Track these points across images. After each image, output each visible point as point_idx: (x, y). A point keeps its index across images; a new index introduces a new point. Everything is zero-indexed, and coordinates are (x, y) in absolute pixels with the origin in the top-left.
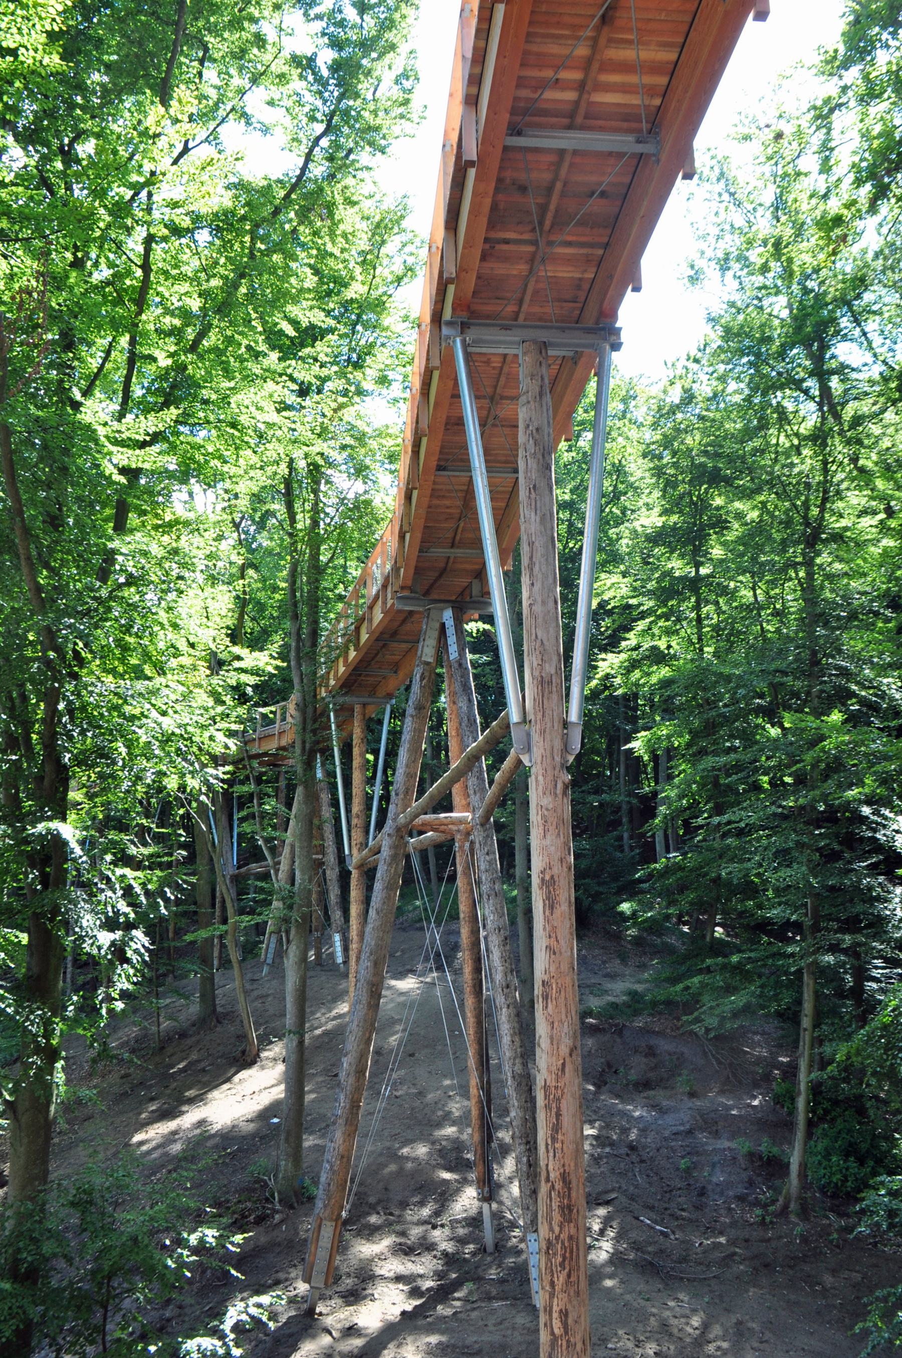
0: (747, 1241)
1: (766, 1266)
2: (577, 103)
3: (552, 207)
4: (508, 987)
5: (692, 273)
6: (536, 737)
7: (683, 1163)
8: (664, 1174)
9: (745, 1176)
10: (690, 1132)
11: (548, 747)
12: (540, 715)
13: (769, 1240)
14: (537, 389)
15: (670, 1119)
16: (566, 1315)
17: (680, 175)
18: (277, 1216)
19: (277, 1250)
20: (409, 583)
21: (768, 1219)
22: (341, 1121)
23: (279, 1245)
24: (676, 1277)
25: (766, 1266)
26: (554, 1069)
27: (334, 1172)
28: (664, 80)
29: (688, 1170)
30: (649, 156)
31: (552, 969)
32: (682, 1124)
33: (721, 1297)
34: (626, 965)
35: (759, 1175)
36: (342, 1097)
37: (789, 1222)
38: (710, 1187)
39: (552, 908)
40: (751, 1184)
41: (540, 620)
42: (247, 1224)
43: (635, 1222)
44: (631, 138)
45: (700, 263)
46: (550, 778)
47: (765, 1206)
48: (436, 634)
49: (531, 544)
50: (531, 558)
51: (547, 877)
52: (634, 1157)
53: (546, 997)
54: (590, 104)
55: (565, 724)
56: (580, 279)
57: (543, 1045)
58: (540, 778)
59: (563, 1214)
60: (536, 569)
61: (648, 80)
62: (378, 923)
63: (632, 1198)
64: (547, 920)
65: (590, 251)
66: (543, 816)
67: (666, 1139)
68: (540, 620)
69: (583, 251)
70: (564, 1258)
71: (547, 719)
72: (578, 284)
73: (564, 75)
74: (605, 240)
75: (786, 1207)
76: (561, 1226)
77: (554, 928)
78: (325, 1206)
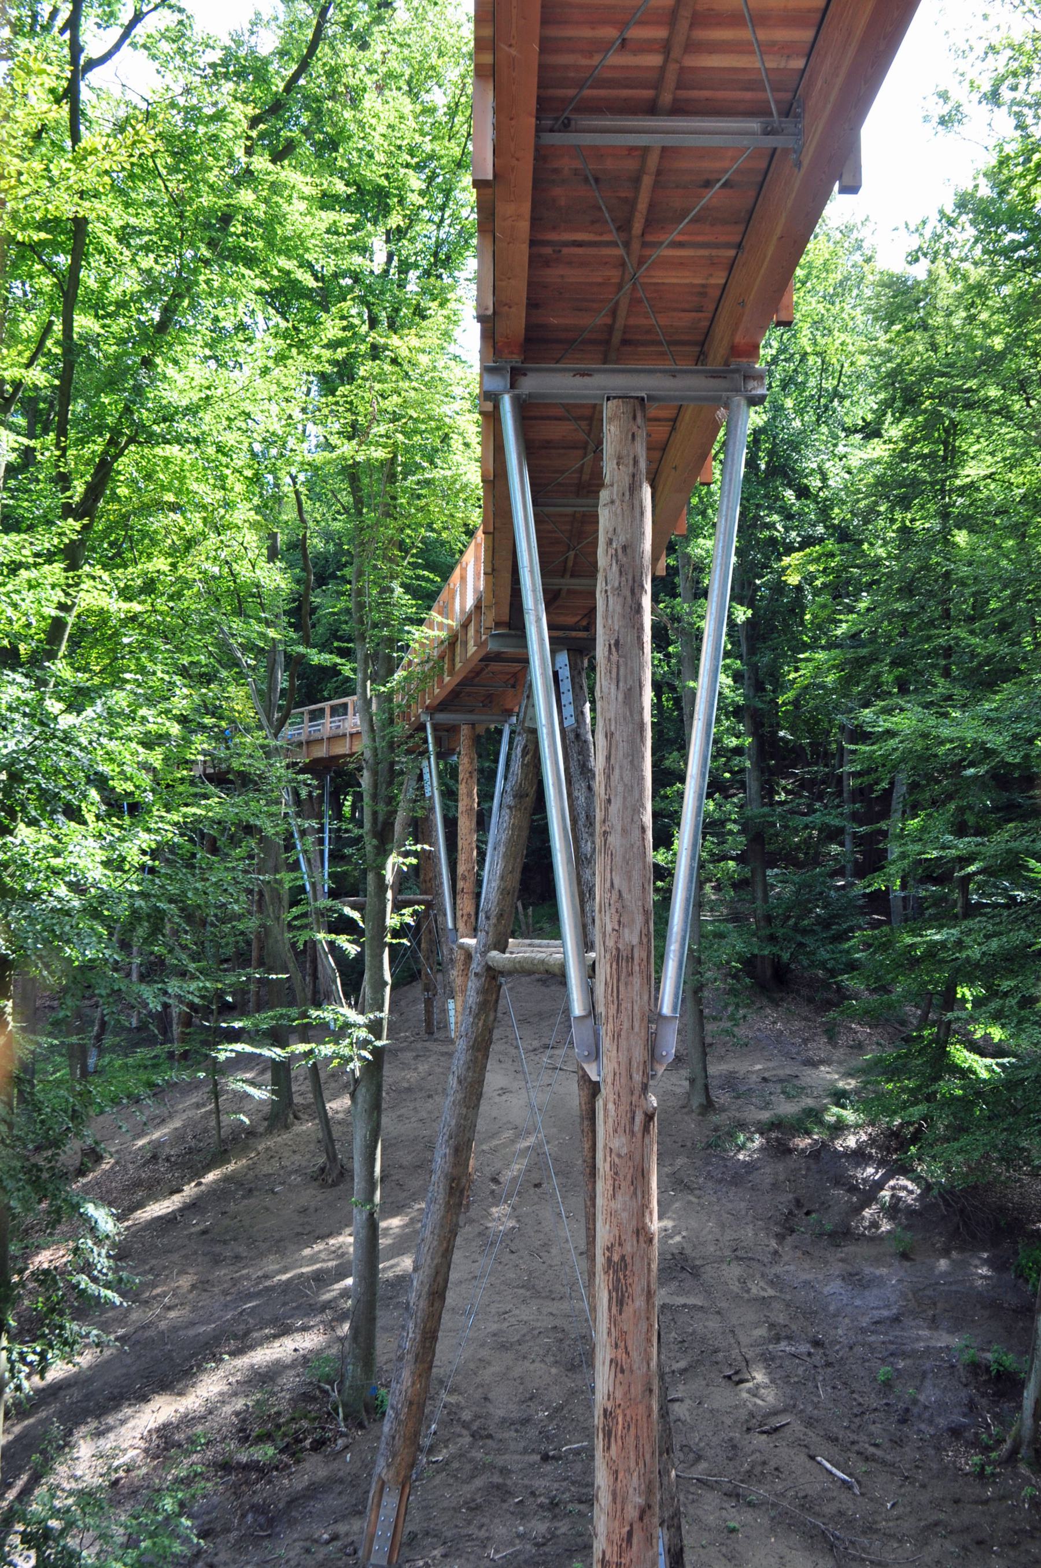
0: (957, 1501)
1: (980, 1543)
2: (663, 69)
3: (642, 206)
5: (945, 110)
6: (606, 1043)
7: (884, 1371)
8: (855, 1385)
9: (963, 1394)
10: (896, 1319)
11: (623, 1059)
12: (613, 1010)
13: (986, 1502)
14: (627, 480)
15: (872, 1297)
17: (836, 187)
18: (340, 1442)
19: (338, 1488)
20: (506, 618)
21: (989, 1469)
22: (409, 1357)
23: (341, 1481)
25: (980, 1543)
26: (616, 1537)
27: (400, 1422)
28: (808, 35)
29: (887, 1384)
30: (786, 151)
31: (619, 1394)
32: (887, 1307)
34: (835, 1046)
35: (984, 1395)
36: (411, 1325)
37: (1017, 1475)
38: (915, 1410)
39: (621, 1303)
40: (971, 1407)
41: (618, 859)
42: (303, 1450)
43: (809, 1464)
44: (754, 125)
45: (959, 94)
46: (624, 1107)
47: (987, 1449)
49: (609, 736)
50: (608, 758)
51: (616, 1258)
53: (608, 1434)
54: (682, 70)
55: (655, 1017)
56: (704, 286)
57: (603, 1501)
58: (611, 1106)
60: (616, 775)
61: (782, 35)
62: (459, 1096)
63: (810, 1423)
64: (613, 1321)
65: (714, 252)
66: (613, 1165)
67: (863, 1331)
68: (618, 859)
69: (705, 252)
71: (624, 1017)
72: (702, 291)
73: (635, 33)
74: (737, 239)
75: (1014, 1451)
77: (623, 1333)
78: (389, 1466)
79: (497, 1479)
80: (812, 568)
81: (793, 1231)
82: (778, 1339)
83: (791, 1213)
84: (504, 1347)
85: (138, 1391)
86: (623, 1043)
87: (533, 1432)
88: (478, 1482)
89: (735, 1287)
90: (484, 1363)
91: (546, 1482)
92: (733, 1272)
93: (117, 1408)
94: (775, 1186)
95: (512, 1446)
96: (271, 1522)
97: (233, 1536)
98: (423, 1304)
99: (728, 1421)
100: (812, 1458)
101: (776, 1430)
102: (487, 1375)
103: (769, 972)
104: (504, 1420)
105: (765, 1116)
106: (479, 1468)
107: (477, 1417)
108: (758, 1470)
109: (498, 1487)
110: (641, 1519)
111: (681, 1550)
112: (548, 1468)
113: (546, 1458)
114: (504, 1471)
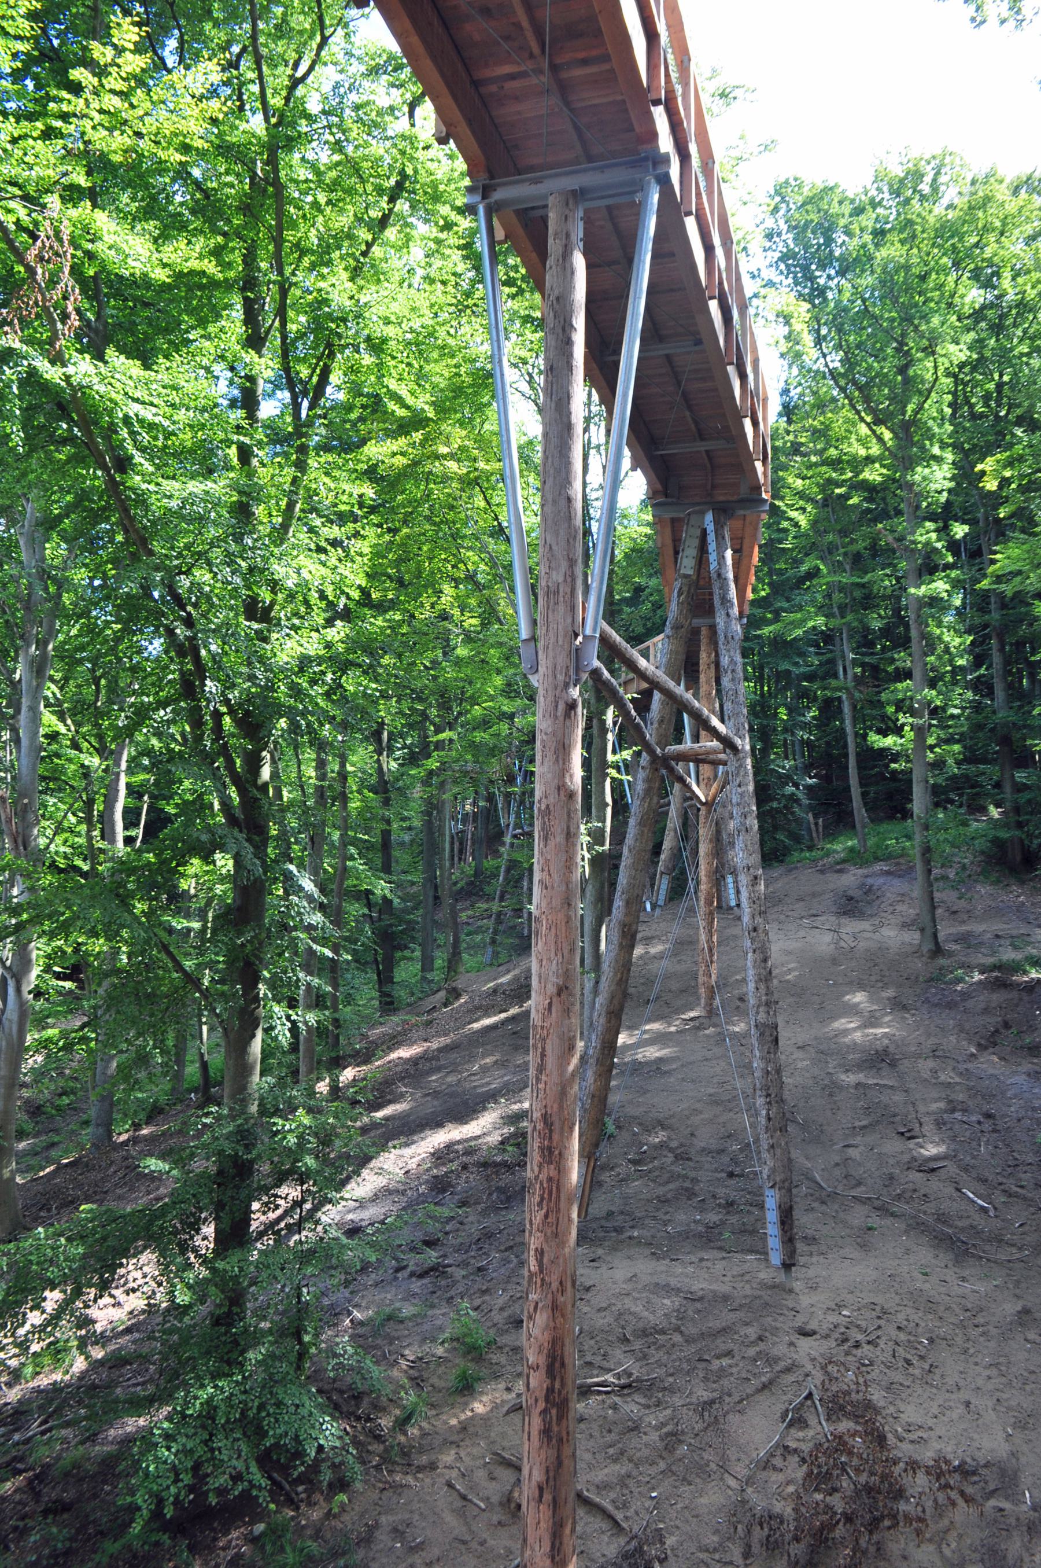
4: (755, 930)
16: (542, 1253)
24: (973, 1255)
33: (1017, 1283)
43: (956, 1194)
46: (550, 698)
48: (696, 542)
52: (987, 1126)
59: (543, 1156)
70: (542, 1199)
76: (540, 1166)
79: (687, 1184)
80: (1007, 474)
81: (995, 1044)
82: (953, 1111)
83: (997, 1031)
84: (716, 1103)
85: (436, 1123)
86: (551, 653)
87: (726, 1159)
88: (671, 1186)
89: (926, 1075)
90: (696, 1112)
91: (727, 1190)
92: (926, 1066)
93: (422, 1131)
94: (986, 1011)
95: (707, 1166)
96: (508, 1199)
97: (479, 1208)
98: (602, 1020)
99: (891, 1161)
100: (959, 1190)
101: (933, 1170)
102: (696, 1120)
103: (1019, 858)
104: (703, 1149)
105: (990, 961)
106: (673, 1177)
107: (682, 1145)
108: (908, 1195)
109: (687, 1189)
110: (559, 995)
111: (791, 1208)
112: (732, 1182)
113: (731, 1175)
114: (695, 1181)
